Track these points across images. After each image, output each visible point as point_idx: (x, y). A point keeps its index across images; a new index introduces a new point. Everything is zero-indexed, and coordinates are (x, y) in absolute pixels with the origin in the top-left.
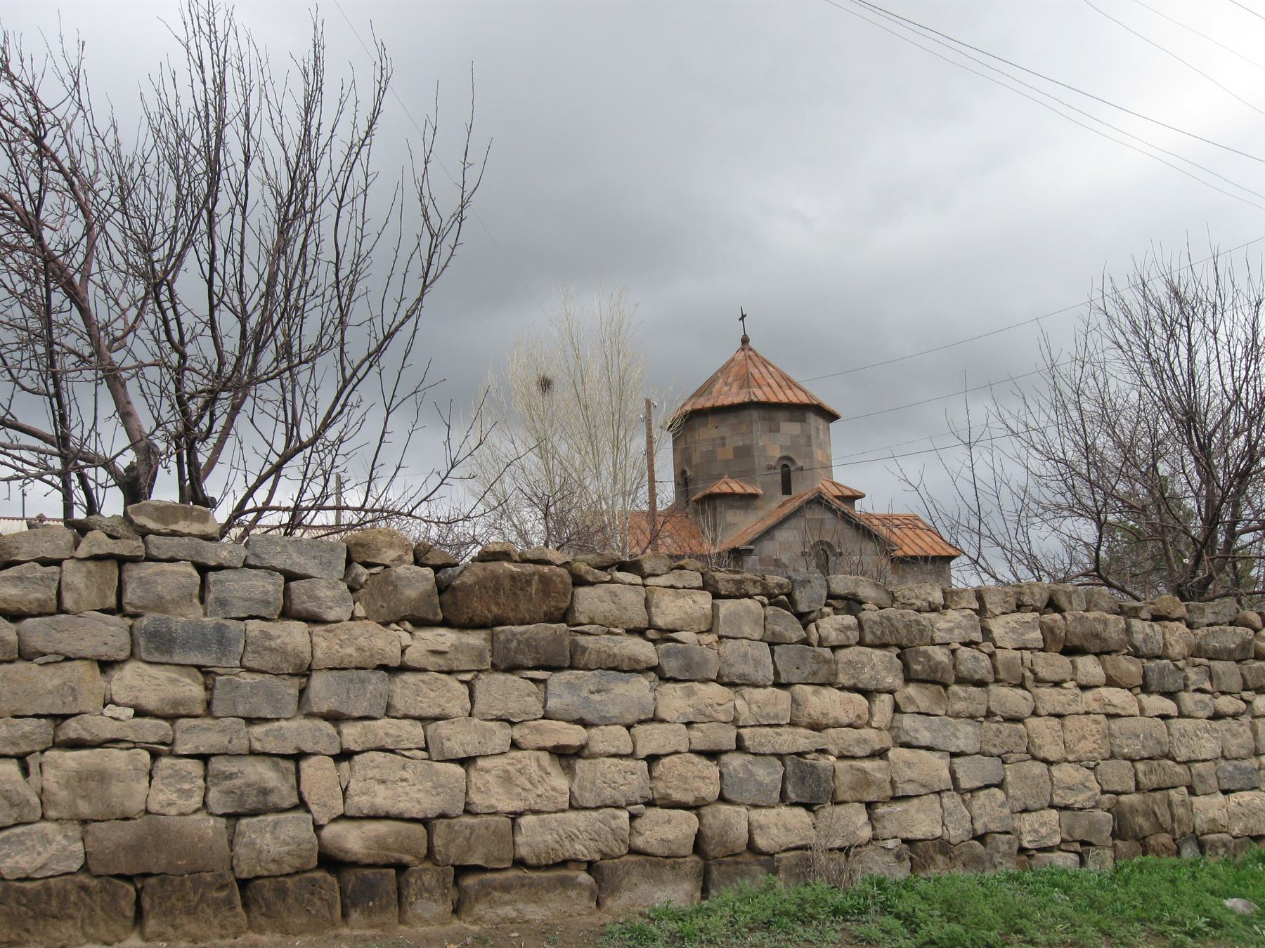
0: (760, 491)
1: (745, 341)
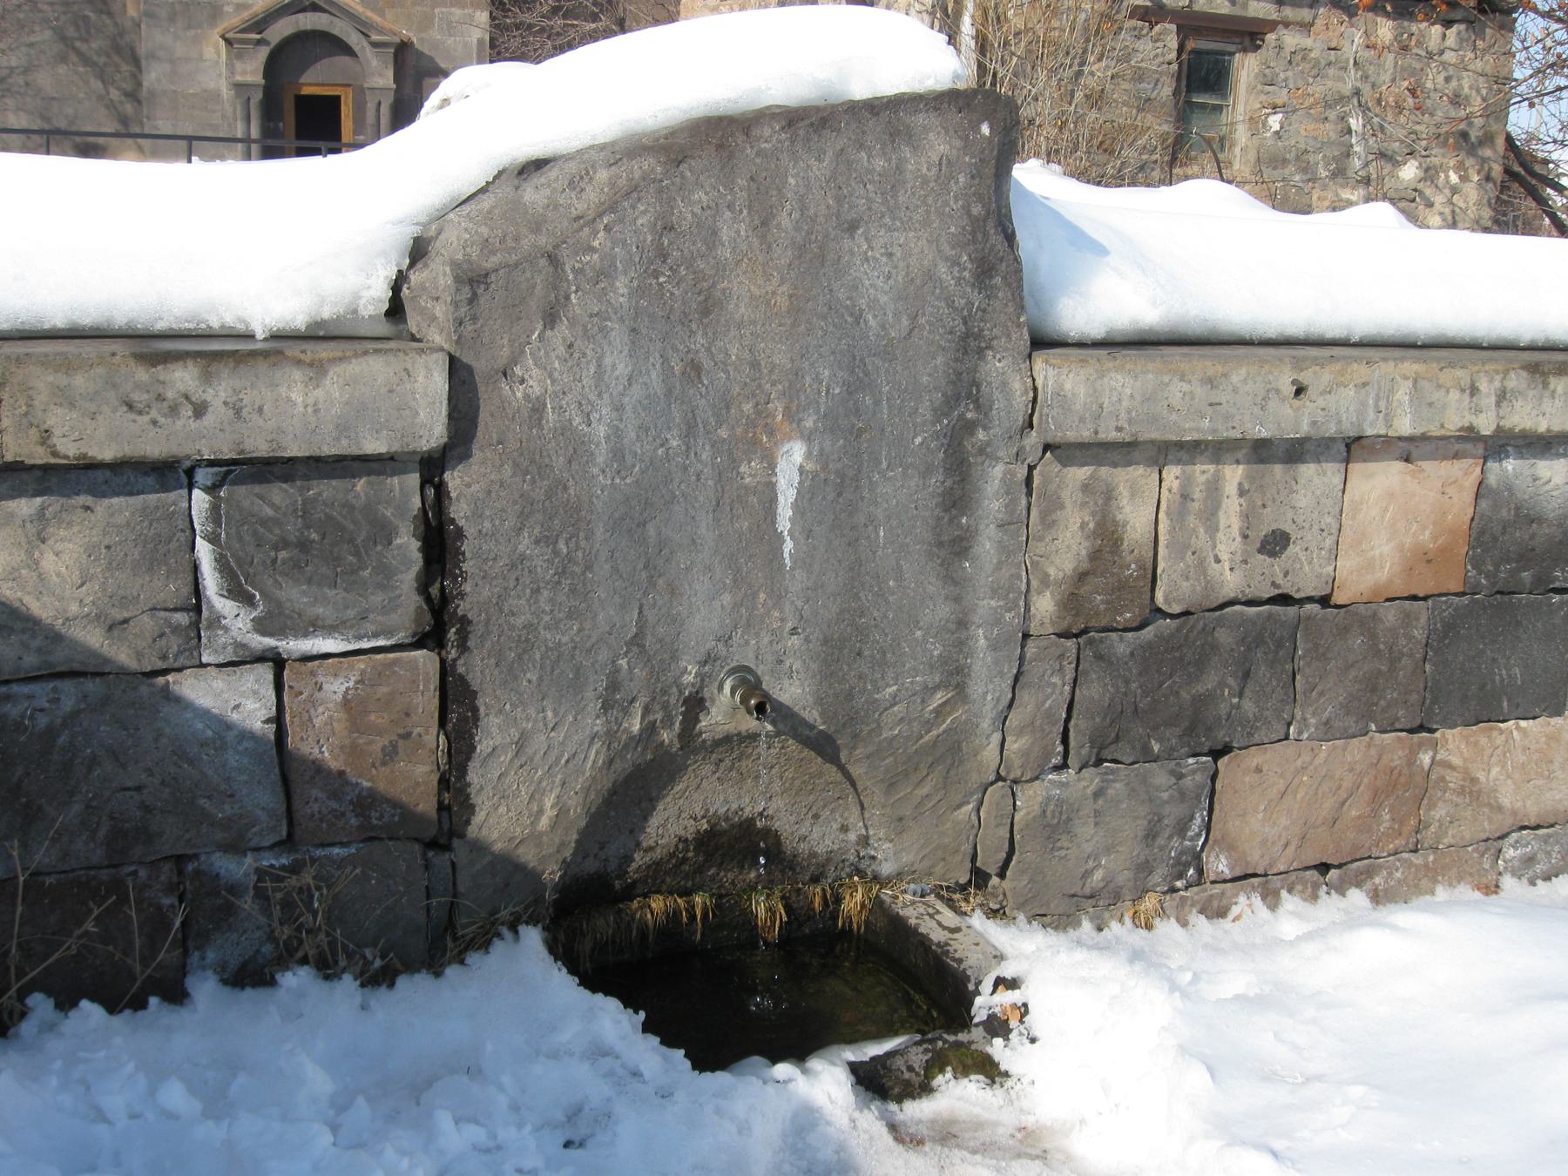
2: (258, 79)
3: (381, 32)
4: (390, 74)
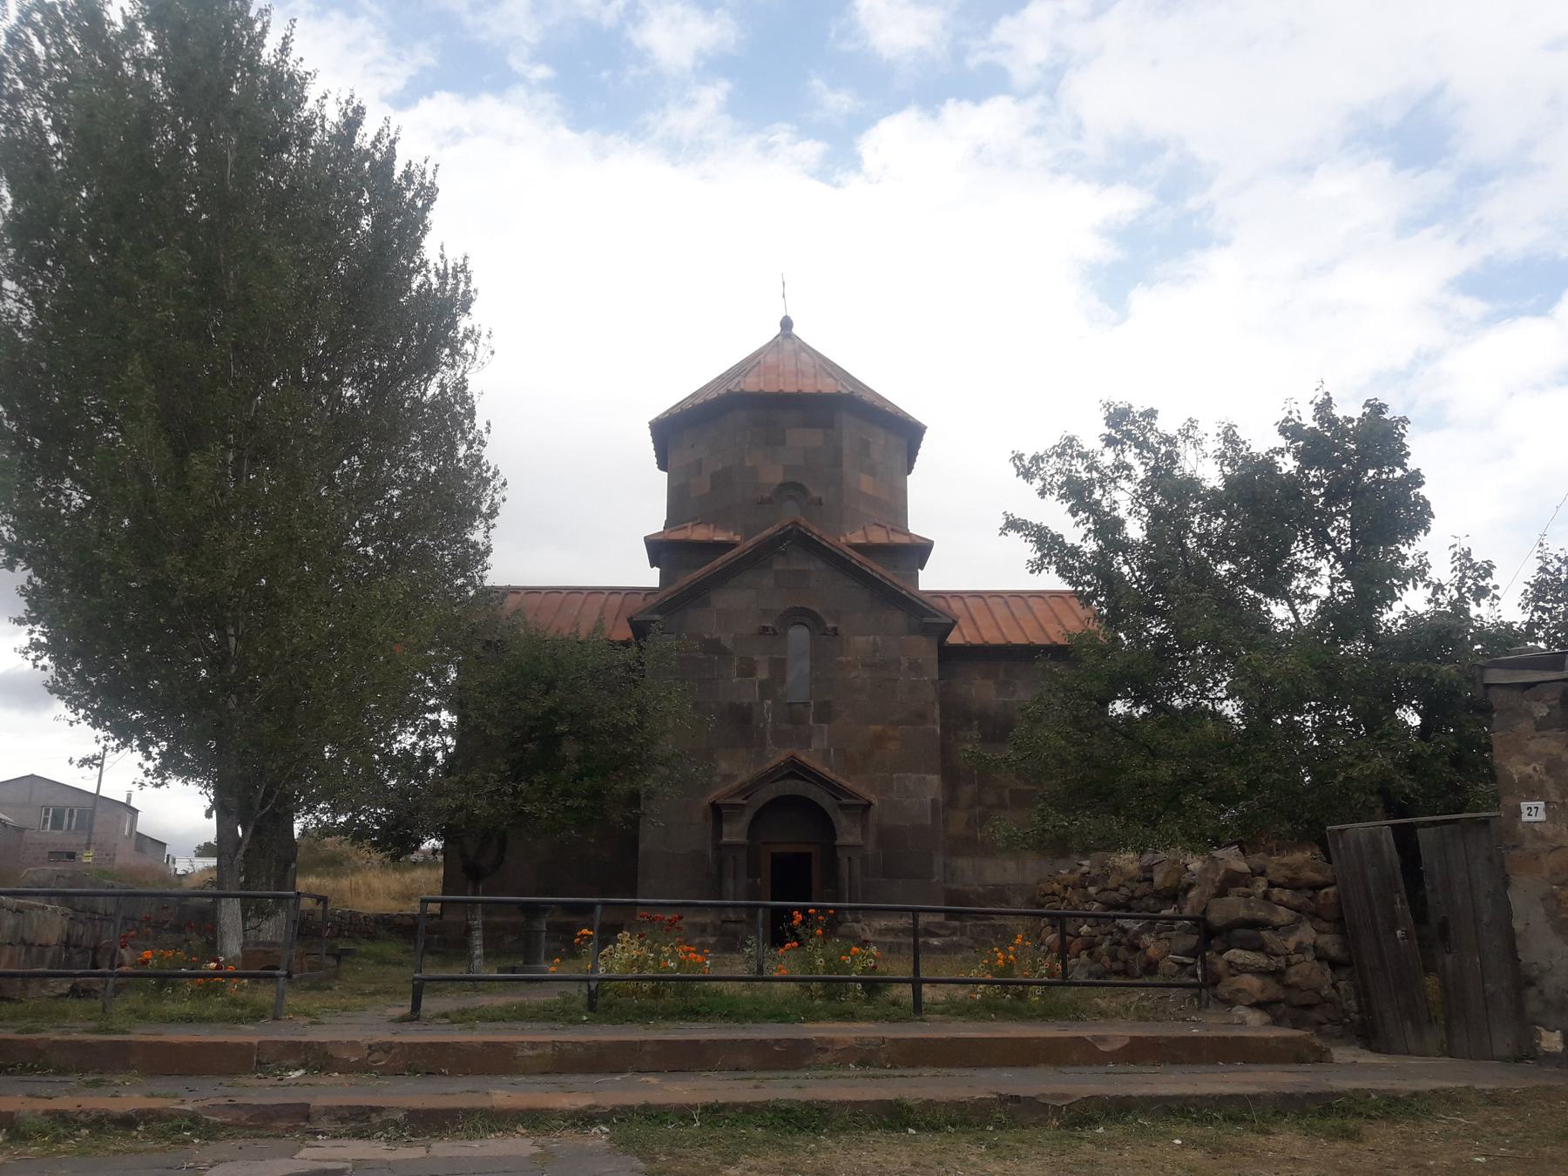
0: (738, 538)
1: (786, 324)
2: (742, 839)
3: (851, 797)
4: (858, 831)
